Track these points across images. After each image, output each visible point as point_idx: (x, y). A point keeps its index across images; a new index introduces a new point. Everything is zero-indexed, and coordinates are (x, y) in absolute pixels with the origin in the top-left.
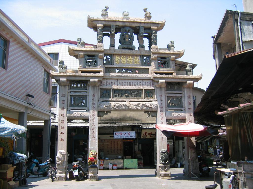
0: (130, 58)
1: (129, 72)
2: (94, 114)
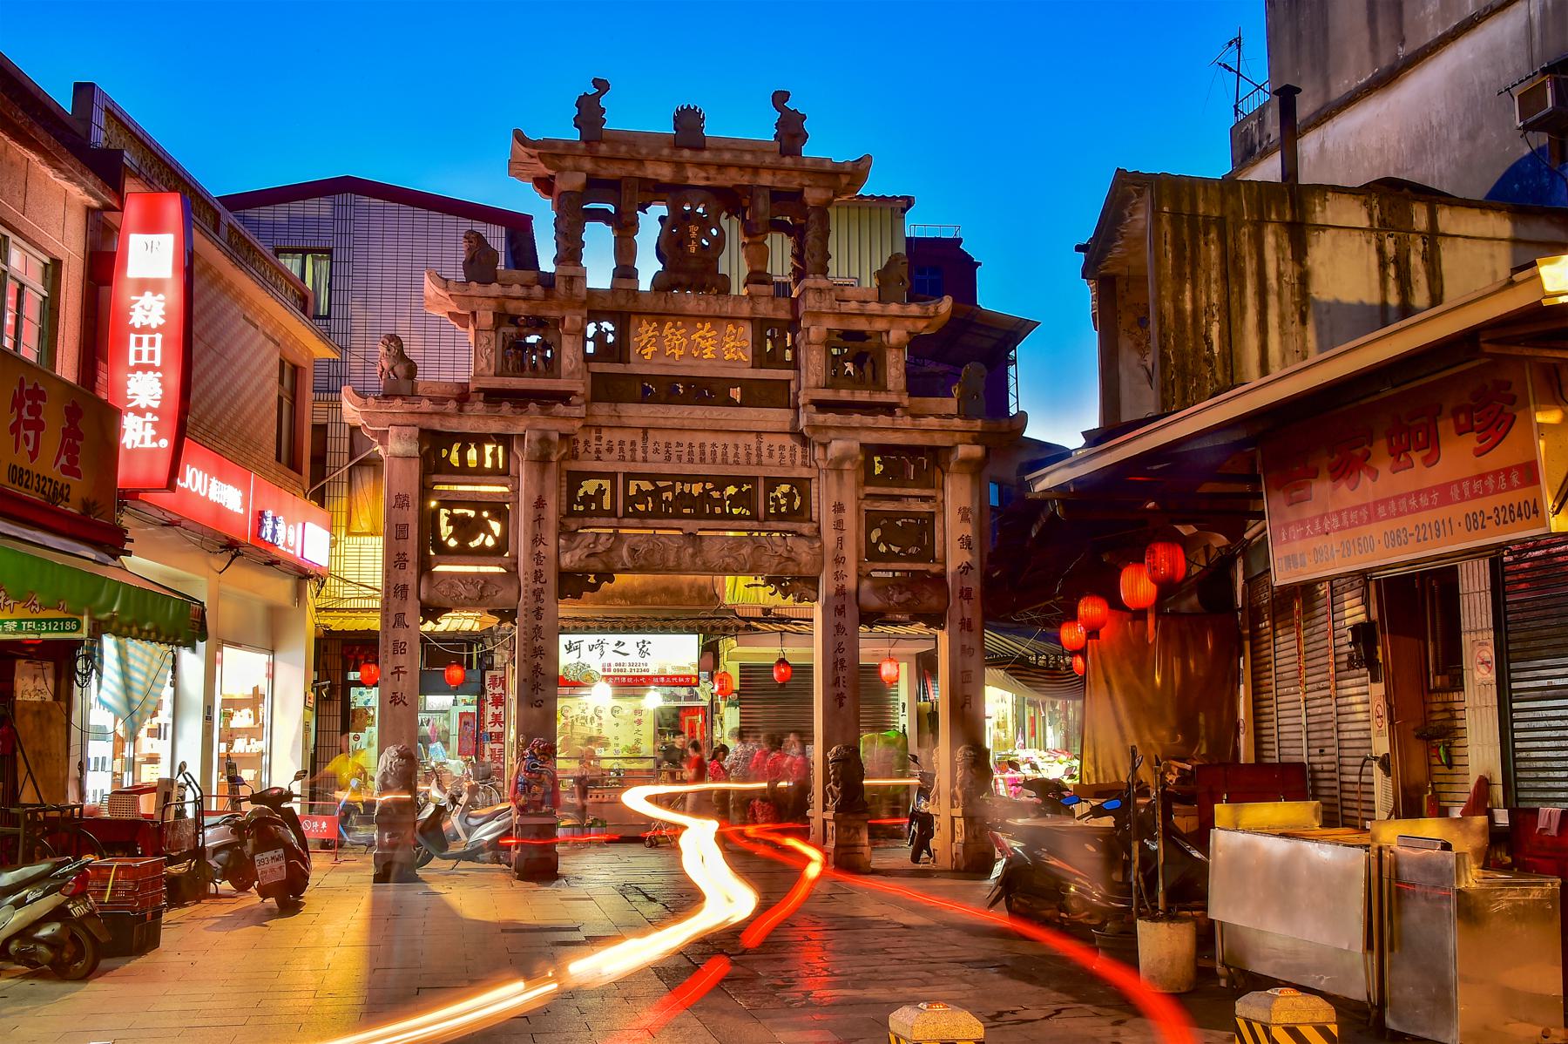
2: (539, 585)
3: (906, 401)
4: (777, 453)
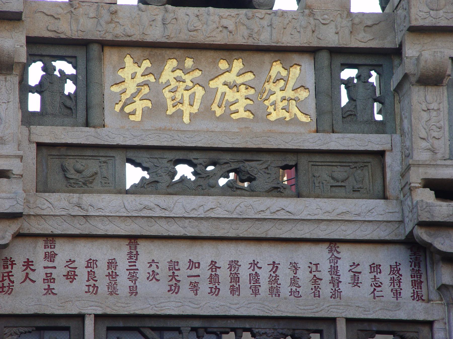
0: (230, 77)
1: (222, 182)
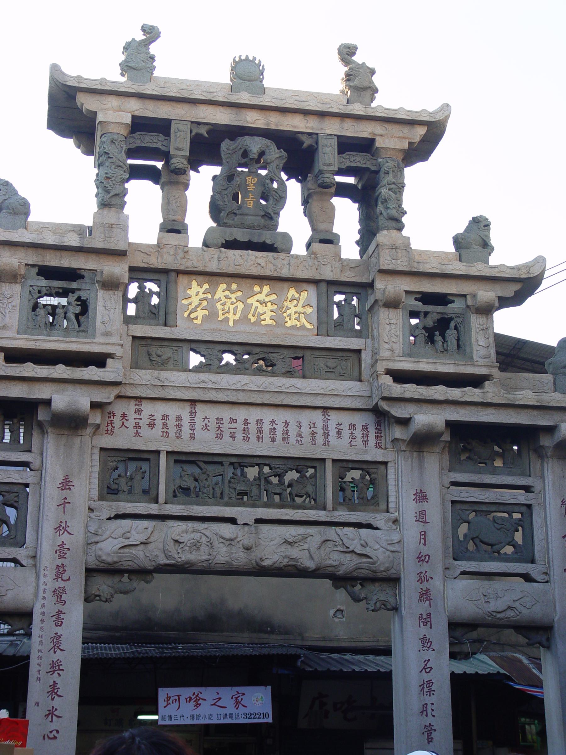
2: (61, 584)
3: (496, 372)
4: (346, 433)
